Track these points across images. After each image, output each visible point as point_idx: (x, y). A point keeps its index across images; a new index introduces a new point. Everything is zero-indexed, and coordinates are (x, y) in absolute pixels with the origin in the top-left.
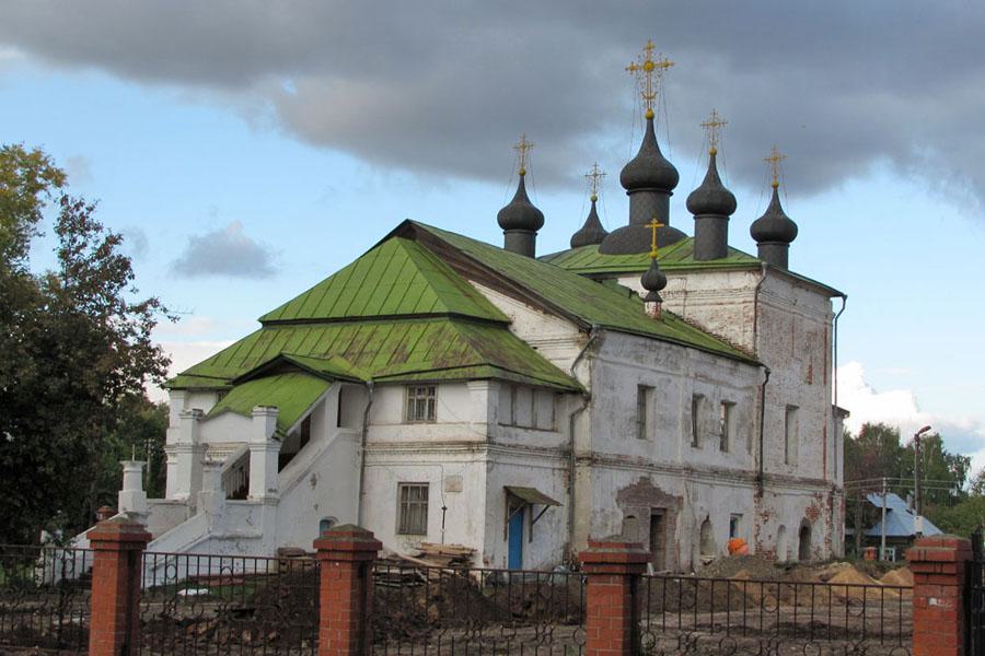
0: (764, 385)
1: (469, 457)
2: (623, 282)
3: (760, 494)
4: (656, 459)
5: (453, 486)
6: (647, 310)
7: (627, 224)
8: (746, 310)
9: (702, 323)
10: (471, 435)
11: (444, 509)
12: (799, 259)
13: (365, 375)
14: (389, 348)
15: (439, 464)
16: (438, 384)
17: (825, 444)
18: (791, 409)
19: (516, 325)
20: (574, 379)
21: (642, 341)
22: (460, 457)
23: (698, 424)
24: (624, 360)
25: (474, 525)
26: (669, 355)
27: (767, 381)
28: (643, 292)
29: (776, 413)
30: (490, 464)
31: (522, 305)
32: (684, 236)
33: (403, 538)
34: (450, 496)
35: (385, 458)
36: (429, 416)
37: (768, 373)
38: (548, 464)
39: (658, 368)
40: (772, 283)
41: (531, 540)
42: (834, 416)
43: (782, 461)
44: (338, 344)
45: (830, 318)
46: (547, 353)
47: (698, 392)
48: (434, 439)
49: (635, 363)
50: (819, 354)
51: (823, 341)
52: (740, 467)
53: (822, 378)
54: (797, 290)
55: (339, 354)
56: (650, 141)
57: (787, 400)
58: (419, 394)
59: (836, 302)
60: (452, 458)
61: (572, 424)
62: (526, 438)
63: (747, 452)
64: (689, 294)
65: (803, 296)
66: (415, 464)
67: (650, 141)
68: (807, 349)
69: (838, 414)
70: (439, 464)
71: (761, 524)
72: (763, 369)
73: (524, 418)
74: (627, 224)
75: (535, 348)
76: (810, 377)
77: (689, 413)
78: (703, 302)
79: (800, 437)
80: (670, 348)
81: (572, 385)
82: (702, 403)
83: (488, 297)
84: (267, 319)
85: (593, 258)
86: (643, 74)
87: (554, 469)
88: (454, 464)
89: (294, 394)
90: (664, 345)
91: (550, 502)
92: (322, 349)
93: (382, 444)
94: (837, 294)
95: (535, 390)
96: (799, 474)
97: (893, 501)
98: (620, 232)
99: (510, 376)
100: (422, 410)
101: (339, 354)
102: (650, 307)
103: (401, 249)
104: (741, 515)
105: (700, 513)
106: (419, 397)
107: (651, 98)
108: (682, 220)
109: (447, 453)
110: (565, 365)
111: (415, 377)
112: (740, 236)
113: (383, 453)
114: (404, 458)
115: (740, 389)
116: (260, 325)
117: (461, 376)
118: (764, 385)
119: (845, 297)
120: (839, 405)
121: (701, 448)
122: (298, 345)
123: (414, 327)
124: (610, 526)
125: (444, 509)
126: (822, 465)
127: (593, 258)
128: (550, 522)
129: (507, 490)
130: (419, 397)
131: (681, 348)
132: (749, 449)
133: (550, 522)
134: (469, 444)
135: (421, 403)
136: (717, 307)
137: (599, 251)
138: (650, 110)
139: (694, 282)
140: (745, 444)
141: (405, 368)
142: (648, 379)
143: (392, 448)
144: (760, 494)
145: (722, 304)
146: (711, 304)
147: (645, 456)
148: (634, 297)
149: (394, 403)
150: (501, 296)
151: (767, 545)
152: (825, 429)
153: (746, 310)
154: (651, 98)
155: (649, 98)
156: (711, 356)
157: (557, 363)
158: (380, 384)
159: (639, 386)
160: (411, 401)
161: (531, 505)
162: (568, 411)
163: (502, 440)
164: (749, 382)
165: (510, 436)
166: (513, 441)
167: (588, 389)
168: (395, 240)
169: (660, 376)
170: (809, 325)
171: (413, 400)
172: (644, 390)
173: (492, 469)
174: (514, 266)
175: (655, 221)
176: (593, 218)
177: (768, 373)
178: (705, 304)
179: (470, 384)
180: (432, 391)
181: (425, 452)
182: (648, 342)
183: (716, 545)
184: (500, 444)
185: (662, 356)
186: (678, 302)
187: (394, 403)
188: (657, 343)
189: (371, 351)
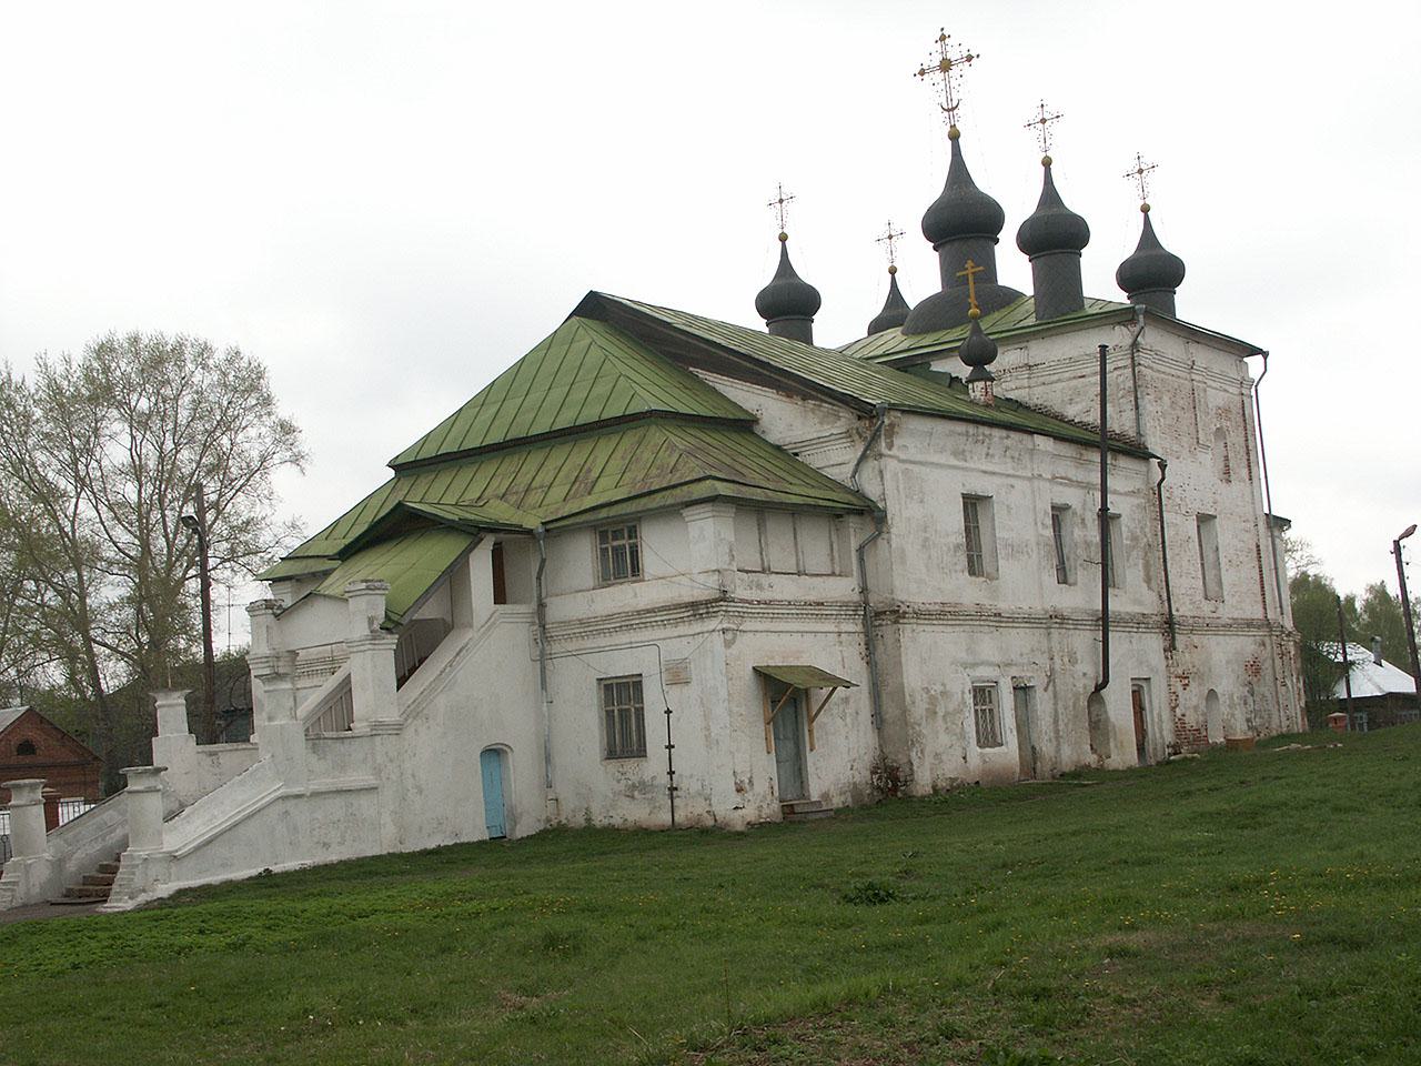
0: (1159, 485)
1: (697, 627)
2: (938, 366)
3: (1171, 648)
4: (1004, 606)
5: (677, 675)
6: (972, 395)
7: (938, 289)
8: (1121, 379)
9: (1057, 408)
10: (696, 592)
11: (668, 712)
12: (1190, 305)
13: (532, 522)
14: (567, 477)
15: (652, 644)
16: (640, 519)
17: (1260, 567)
18: (1204, 520)
19: (765, 421)
20: (858, 493)
21: (960, 427)
22: (683, 629)
23: (1066, 551)
24: (936, 458)
25: (715, 731)
26: (1007, 448)
27: (1163, 479)
28: (964, 371)
29: (1181, 527)
30: (729, 636)
31: (771, 393)
32: (1019, 295)
33: (613, 765)
34: (675, 692)
35: (572, 646)
36: (633, 571)
37: (1163, 466)
38: (829, 626)
39: (990, 468)
40: (1152, 338)
41: (811, 750)
42: (1269, 527)
43: (1199, 596)
44: (495, 483)
45: (1247, 386)
46: (815, 460)
47: (1059, 501)
48: (641, 606)
49: (956, 462)
50: (1236, 438)
51: (1240, 420)
52: (1137, 609)
53: (1245, 472)
54: (1193, 348)
55: (497, 497)
56: (958, 172)
57: (1197, 507)
58: (615, 538)
59: (1254, 363)
60: (670, 631)
61: (861, 560)
62: (784, 589)
63: (1145, 585)
64: (1035, 370)
65: (1202, 356)
66: (616, 648)
67: (958, 172)
68: (1220, 433)
69: (1276, 524)
70: (652, 644)
71: (1179, 689)
72: (1155, 462)
73: (780, 556)
74: (938, 289)
75: (796, 454)
76: (1227, 473)
77: (1049, 532)
78: (1056, 377)
79: (1223, 561)
80: (1008, 437)
81: (855, 501)
82: (1067, 518)
83: (718, 387)
84: (399, 462)
85: (894, 340)
86: (939, 76)
87: (839, 633)
88: (677, 642)
89: (419, 561)
90: (997, 433)
91: (835, 682)
92: (473, 494)
93: (566, 623)
94: (1255, 351)
95: (796, 512)
96: (1227, 612)
97: (1356, 653)
98: (930, 305)
99: (747, 493)
100: (623, 564)
101: (497, 497)
102: (977, 391)
103: (591, 334)
104: (1148, 680)
105: (1084, 681)
106: (615, 543)
107: (953, 109)
108: (1014, 269)
109: (664, 624)
110: (842, 474)
111: (603, 513)
112: (1099, 279)
113: (570, 638)
114: (602, 641)
115: (1127, 494)
116: (391, 473)
117: (670, 501)
118: (1159, 485)
119: (1265, 355)
120: (1273, 513)
121: (1075, 584)
122: (438, 496)
123: (602, 442)
124: (941, 714)
125: (668, 712)
126: (1260, 598)
127: (894, 340)
128: (843, 718)
129: (754, 668)
130: (615, 543)
131: (1025, 437)
132: (1148, 580)
133: (843, 718)
134: (694, 605)
135: (618, 551)
136: (1075, 382)
137: (903, 334)
138: (953, 126)
139: (1041, 351)
140: (1142, 574)
141: (589, 502)
142: (979, 486)
143: (590, 627)
144: (1171, 648)
145: (1083, 376)
146: (1070, 379)
147: (986, 602)
148: (955, 385)
149: (581, 557)
150: (739, 384)
151: (1192, 720)
152: (1258, 546)
153: (1121, 379)
154: (953, 109)
155: (948, 110)
156: (1073, 446)
157: (831, 473)
158: (557, 530)
159: (965, 496)
160: (604, 551)
161: (807, 691)
162: (854, 544)
163: (747, 595)
164: (1138, 484)
165: (760, 587)
166: (766, 595)
167: (880, 505)
168: (574, 319)
169: (997, 480)
170: (1216, 398)
171: (607, 549)
172: (973, 504)
173: (733, 641)
174: (783, 354)
175: (970, 264)
176: (895, 297)
177: (1163, 466)
178: (1059, 381)
179: (686, 512)
180: (633, 533)
181: (630, 627)
182: (971, 429)
183: (1114, 727)
184: (742, 601)
185: (996, 450)
186: (1018, 383)
187: (581, 557)
188: (987, 430)
189: (541, 487)
